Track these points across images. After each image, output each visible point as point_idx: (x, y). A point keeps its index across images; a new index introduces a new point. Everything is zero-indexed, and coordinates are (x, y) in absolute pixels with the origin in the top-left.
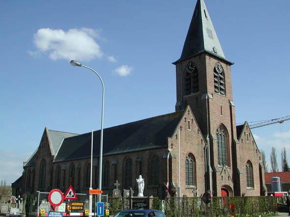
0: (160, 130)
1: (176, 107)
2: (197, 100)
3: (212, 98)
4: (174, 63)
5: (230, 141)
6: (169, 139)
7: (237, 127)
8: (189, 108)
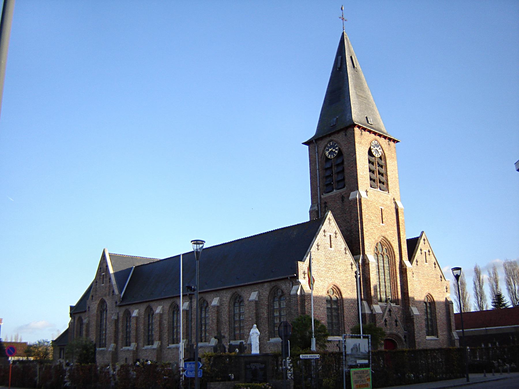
0: (295, 242)
1: (311, 212)
2: (343, 200)
3: (366, 197)
4: (305, 143)
5: (398, 264)
6: (300, 263)
7: (408, 241)
8: (330, 215)
